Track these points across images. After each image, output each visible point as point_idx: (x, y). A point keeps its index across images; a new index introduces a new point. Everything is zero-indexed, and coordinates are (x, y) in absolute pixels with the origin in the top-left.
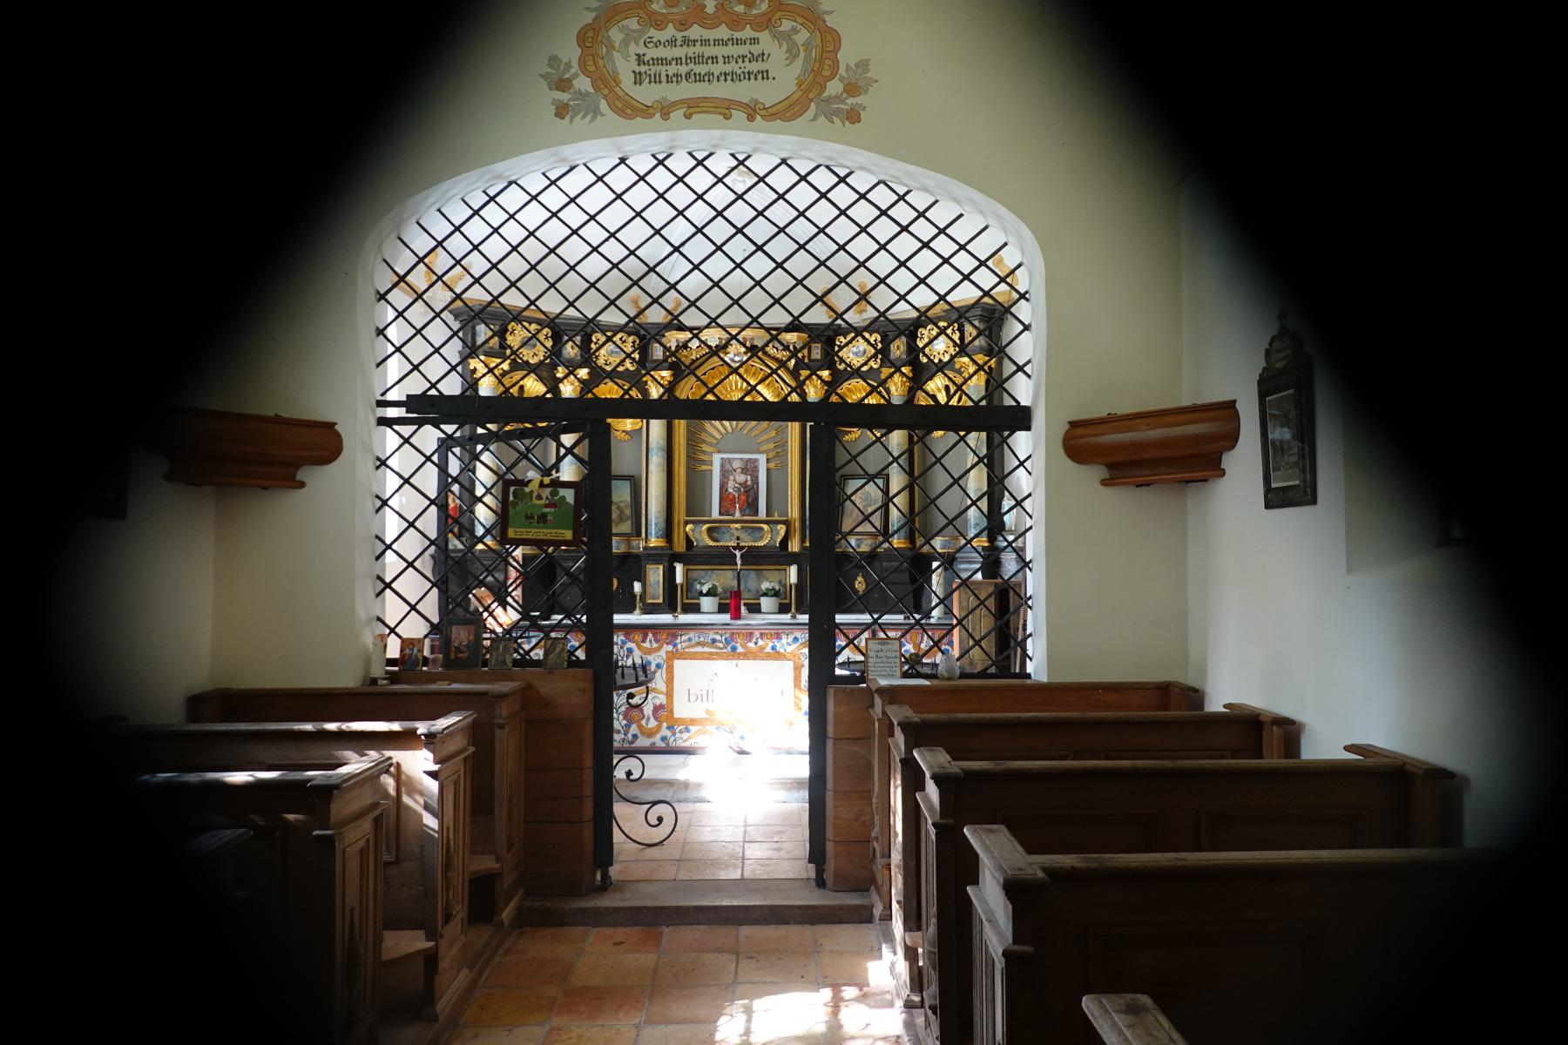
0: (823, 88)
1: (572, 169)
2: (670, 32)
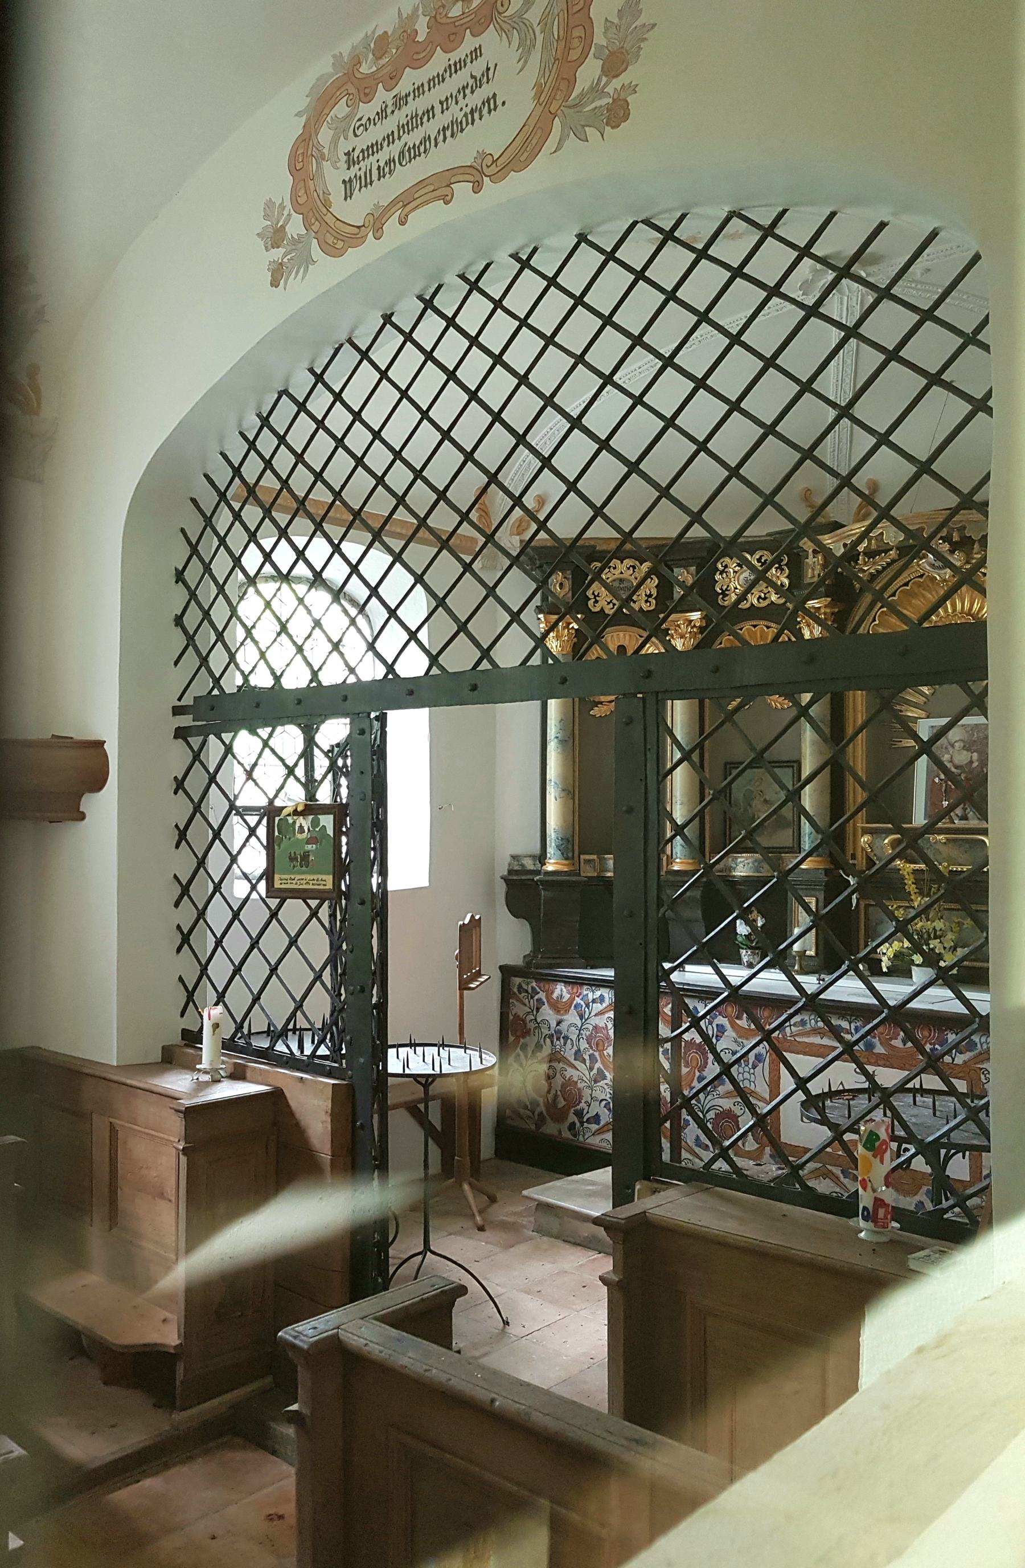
0: (572, 82)
1: (337, 351)
2: (383, 96)
